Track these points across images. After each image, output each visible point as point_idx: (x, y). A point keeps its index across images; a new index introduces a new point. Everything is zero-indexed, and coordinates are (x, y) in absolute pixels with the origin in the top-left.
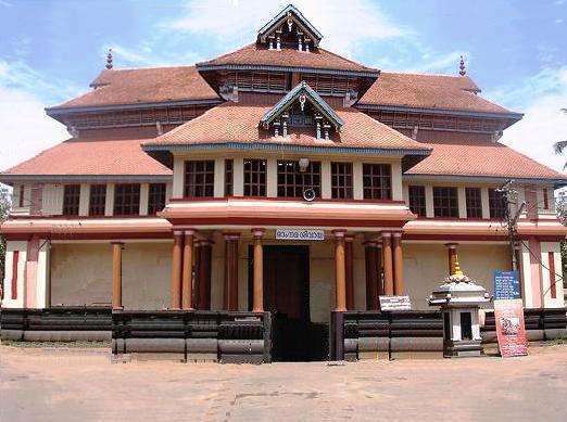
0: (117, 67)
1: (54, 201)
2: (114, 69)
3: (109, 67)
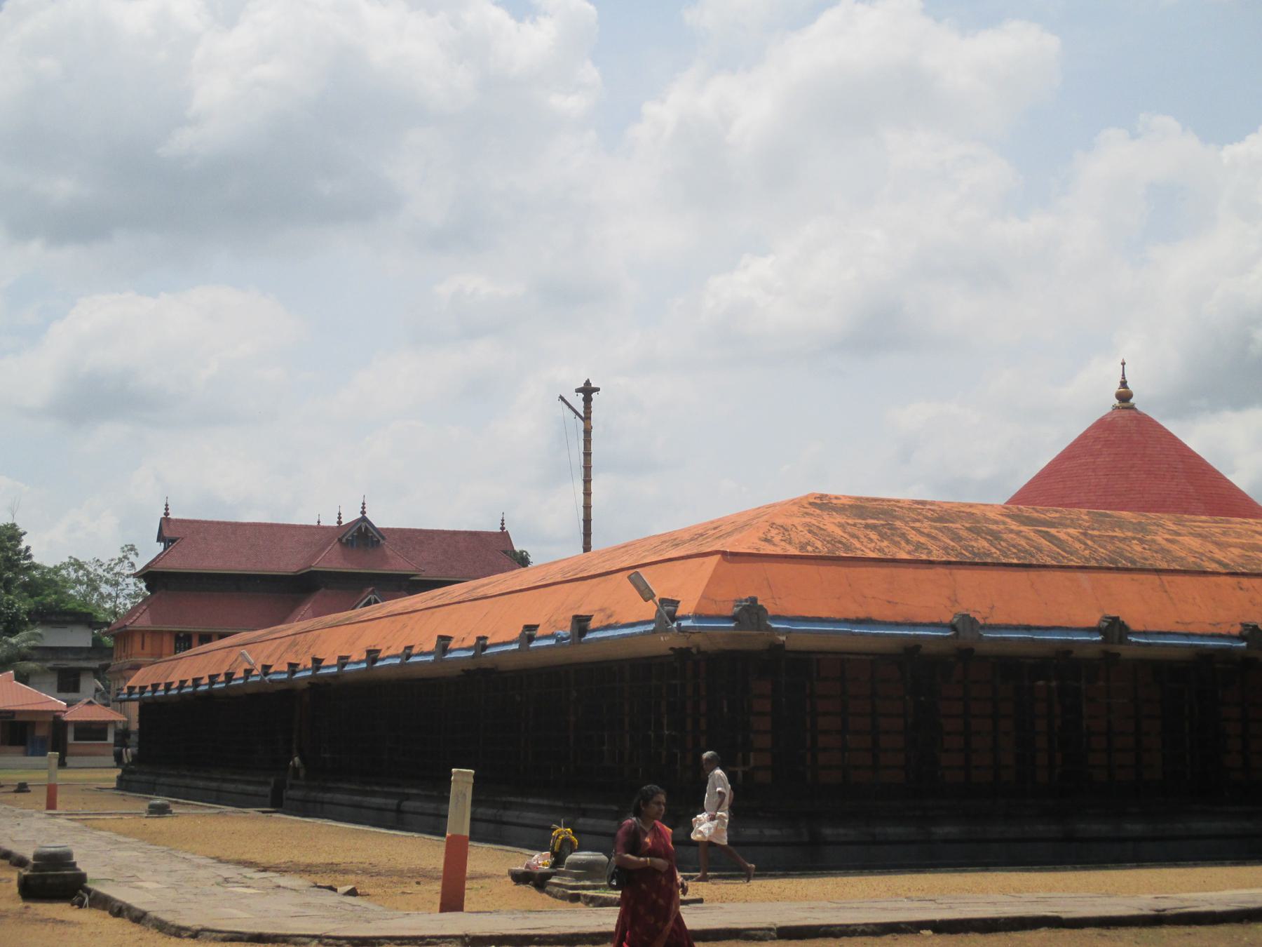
3: (167, 514)
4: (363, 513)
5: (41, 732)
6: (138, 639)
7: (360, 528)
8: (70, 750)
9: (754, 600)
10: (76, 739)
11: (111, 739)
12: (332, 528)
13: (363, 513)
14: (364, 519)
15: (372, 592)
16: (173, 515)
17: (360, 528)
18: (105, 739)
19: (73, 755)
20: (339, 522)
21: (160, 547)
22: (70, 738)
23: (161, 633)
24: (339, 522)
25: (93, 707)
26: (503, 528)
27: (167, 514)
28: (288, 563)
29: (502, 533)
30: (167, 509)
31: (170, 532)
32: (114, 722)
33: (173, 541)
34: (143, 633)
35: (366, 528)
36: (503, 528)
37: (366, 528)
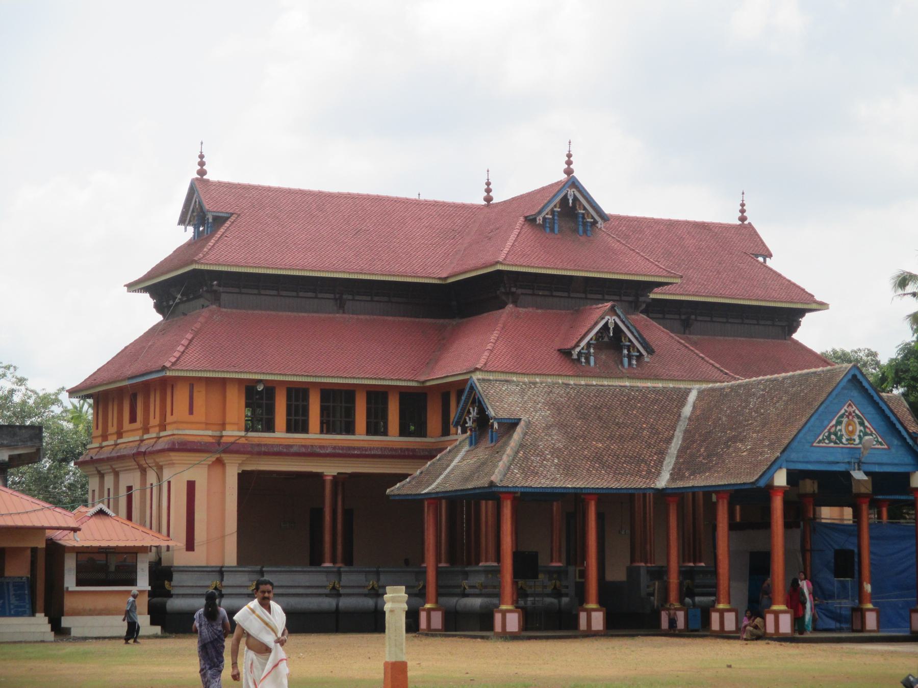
0: (498, 197)
1: (236, 407)
2: (494, 201)
3: (202, 172)
4: (569, 172)
5: (18, 570)
6: (181, 397)
7: (565, 198)
8: (69, 603)
9: (386, 664)
10: (79, 583)
11: (143, 583)
12: (479, 208)
13: (569, 172)
14: (573, 183)
15: (612, 311)
16: (212, 175)
17: (565, 198)
18: (133, 582)
19: (223, 561)
20: (488, 199)
21: (187, 234)
22: (70, 581)
23: (223, 382)
24: (488, 199)
25: (107, 521)
26: (743, 219)
27: (202, 172)
28: (431, 263)
29: (742, 227)
30: (202, 164)
31: (205, 210)
32: (145, 549)
33: (219, 221)
34: (192, 382)
35: (575, 199)
36: (743, 219)
37: (575, 199)
